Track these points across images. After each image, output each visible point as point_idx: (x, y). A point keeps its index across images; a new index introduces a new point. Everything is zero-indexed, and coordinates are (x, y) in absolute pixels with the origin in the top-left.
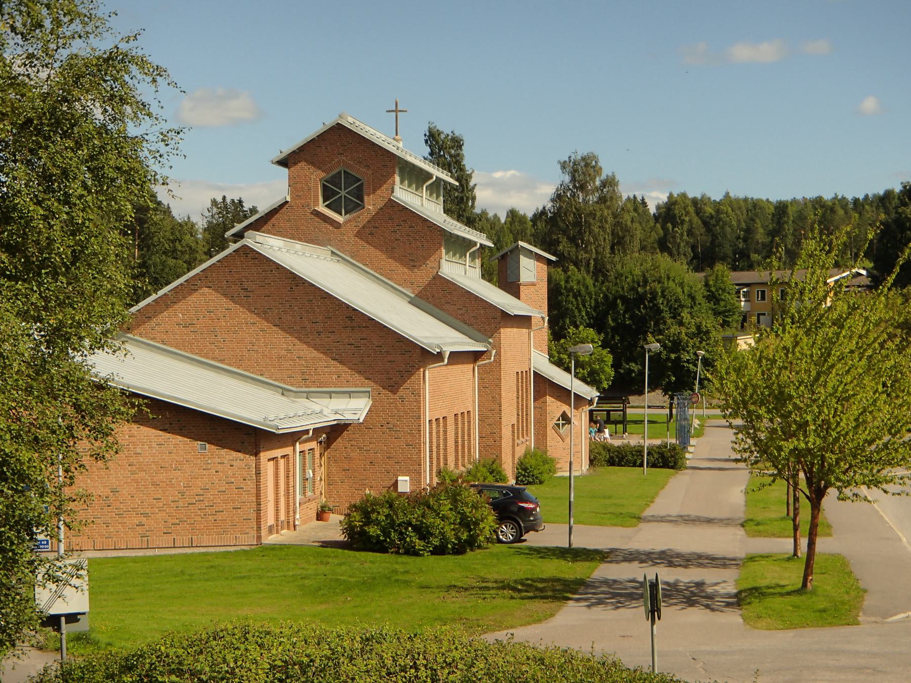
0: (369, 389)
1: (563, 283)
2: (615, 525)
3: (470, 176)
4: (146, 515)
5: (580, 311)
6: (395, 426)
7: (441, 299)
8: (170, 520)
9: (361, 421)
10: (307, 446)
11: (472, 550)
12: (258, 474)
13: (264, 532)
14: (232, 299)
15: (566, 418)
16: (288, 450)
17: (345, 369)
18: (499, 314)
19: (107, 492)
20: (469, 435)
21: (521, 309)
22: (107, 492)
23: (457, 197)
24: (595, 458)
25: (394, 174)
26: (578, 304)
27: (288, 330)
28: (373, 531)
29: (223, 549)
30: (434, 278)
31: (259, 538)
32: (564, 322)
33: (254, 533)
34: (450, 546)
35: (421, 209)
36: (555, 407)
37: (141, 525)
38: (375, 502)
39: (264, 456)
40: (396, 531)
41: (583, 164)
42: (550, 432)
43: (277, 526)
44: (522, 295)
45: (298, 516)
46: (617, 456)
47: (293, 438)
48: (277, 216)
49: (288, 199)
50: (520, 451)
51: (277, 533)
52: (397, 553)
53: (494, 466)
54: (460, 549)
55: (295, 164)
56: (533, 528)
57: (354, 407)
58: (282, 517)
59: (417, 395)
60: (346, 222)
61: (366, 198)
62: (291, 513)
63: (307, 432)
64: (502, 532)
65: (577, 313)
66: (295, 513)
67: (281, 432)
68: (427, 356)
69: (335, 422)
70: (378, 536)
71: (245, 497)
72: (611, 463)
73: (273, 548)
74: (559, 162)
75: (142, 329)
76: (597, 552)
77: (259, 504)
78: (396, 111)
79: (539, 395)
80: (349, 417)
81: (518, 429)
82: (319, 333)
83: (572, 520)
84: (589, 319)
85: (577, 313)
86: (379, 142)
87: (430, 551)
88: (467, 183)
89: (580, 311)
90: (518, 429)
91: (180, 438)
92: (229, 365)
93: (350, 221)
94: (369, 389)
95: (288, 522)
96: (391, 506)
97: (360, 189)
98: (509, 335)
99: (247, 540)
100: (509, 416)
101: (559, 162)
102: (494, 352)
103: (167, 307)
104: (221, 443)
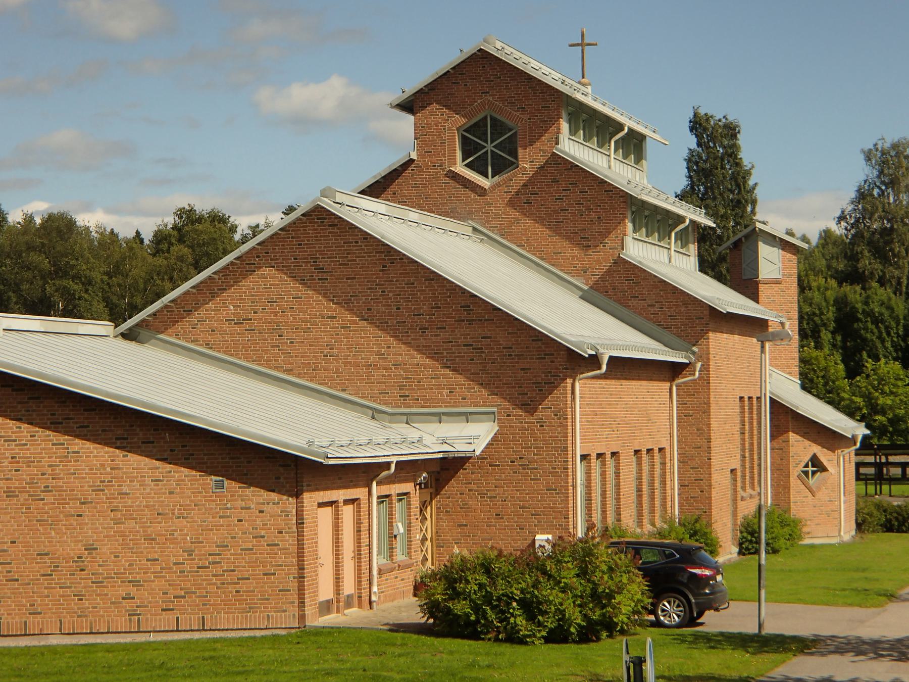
0: (495, 409)
1: (859, 306)
2: (850, 605)
3: (748, 173)
4: (135, 583)
5: (883, 341)
6: (531, 459)
7: (627, 292)
8: (171, 590)
9: (478, 453)
10: (395, 489)
11: (610, 636)
12: (300, 523)
13: (309, 611)
14: (303, 282)
15: (817, 464)
16: (359, 493)
17: (461, 379)
18: (707, 312)
19: (80, 549)
20: (663, 482)
21: (755, 310)
22: (80, 549)
23: (732, 201)
24: (864, 521)
25: (559, 117)
26: (880, 332)
27: (383, 325)
28: (460, 607)
29: (247, 634)
30: (615, 262)
31: (302, 617)
32: (861, 356)
33: (294, 610)
34: (572, 630)
35: (607, 172)
36: (801, 448)
37: (128, 597)
38: (464, 564)
39: (310, 499)
40: (493, 608)
41: (893, 153)
42: (795, 483)
43: (338, 601)
44: (762, 297)
45: (375, 589)
46: (897, 519)
47: (363, 473)
48: (400, 180)
49: (414, 156)
50: (747, 508)
51: (338, 611)
52: (497, 640)
53: (698, 525)
54: (588, 634)
55: (423, 108)
56: (711, 604)
57: (472, 435)
58: (349, 587)
59: (562, 416)
60: (493, 187)
61: (520, 151)
62: (365, 584)
63: (387, 465)
64: (663, 611)
65: (879, 345)
66: (370, 584)
67: (332, 462)
68: (578, 362)
69: (440, 455)
70: (468, 615)
71: (281, 558)
72: (888, 527)
73: (319, 632)
74: (863, 151)
75: (178, 327)
76: (795, 639)
77: (301, 568)
78: (582, 45)
79: (778, 431)
80: (461, 448)
81: (744, 476)
82: (423, 329)
83: (763, 592)
84: (896, 351)
85: (879, 345)
86: (548, 80)
87: (543, 637)
88: (745, 182)
89: (883, 341)
90: (744, 476)
91: (186, 471)
92: (299, 376)
93: (498, 185)
94: (495, 409)
95: (360, 597)
96: (488, 571)
97: (513, 140)
98: (721, 344)
99: (283, 621)
100: (725, 455)
101: (863, 151)
102: (699, 365)
103: (213, 295)
104: (247, 479)
